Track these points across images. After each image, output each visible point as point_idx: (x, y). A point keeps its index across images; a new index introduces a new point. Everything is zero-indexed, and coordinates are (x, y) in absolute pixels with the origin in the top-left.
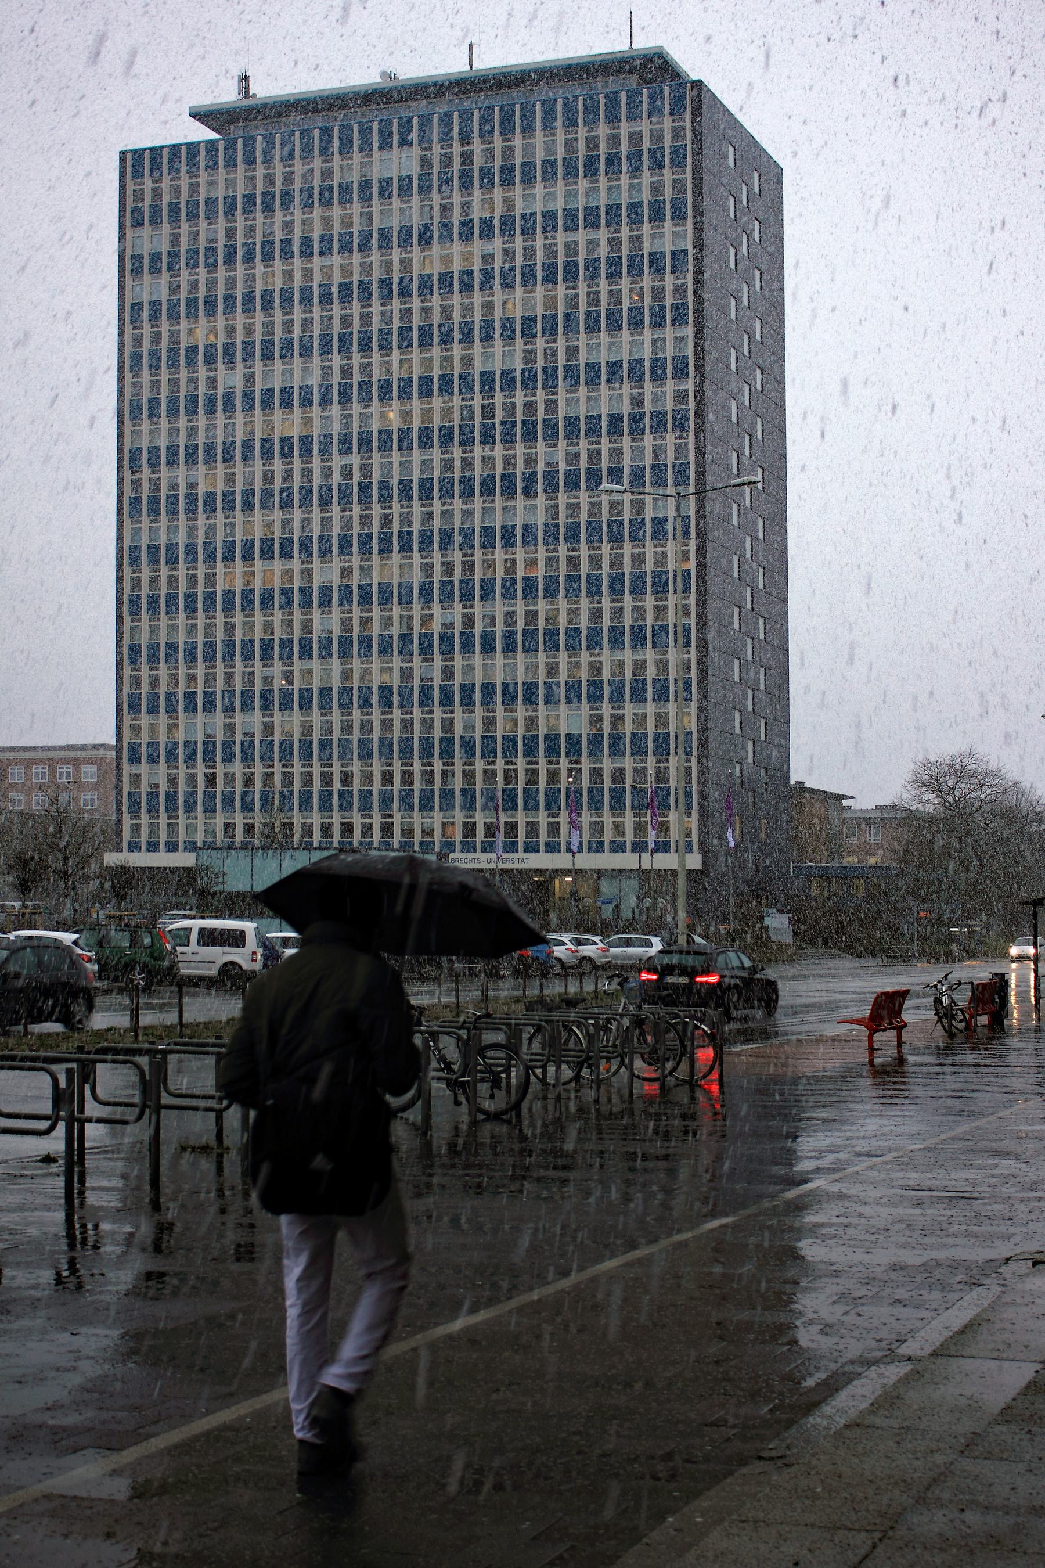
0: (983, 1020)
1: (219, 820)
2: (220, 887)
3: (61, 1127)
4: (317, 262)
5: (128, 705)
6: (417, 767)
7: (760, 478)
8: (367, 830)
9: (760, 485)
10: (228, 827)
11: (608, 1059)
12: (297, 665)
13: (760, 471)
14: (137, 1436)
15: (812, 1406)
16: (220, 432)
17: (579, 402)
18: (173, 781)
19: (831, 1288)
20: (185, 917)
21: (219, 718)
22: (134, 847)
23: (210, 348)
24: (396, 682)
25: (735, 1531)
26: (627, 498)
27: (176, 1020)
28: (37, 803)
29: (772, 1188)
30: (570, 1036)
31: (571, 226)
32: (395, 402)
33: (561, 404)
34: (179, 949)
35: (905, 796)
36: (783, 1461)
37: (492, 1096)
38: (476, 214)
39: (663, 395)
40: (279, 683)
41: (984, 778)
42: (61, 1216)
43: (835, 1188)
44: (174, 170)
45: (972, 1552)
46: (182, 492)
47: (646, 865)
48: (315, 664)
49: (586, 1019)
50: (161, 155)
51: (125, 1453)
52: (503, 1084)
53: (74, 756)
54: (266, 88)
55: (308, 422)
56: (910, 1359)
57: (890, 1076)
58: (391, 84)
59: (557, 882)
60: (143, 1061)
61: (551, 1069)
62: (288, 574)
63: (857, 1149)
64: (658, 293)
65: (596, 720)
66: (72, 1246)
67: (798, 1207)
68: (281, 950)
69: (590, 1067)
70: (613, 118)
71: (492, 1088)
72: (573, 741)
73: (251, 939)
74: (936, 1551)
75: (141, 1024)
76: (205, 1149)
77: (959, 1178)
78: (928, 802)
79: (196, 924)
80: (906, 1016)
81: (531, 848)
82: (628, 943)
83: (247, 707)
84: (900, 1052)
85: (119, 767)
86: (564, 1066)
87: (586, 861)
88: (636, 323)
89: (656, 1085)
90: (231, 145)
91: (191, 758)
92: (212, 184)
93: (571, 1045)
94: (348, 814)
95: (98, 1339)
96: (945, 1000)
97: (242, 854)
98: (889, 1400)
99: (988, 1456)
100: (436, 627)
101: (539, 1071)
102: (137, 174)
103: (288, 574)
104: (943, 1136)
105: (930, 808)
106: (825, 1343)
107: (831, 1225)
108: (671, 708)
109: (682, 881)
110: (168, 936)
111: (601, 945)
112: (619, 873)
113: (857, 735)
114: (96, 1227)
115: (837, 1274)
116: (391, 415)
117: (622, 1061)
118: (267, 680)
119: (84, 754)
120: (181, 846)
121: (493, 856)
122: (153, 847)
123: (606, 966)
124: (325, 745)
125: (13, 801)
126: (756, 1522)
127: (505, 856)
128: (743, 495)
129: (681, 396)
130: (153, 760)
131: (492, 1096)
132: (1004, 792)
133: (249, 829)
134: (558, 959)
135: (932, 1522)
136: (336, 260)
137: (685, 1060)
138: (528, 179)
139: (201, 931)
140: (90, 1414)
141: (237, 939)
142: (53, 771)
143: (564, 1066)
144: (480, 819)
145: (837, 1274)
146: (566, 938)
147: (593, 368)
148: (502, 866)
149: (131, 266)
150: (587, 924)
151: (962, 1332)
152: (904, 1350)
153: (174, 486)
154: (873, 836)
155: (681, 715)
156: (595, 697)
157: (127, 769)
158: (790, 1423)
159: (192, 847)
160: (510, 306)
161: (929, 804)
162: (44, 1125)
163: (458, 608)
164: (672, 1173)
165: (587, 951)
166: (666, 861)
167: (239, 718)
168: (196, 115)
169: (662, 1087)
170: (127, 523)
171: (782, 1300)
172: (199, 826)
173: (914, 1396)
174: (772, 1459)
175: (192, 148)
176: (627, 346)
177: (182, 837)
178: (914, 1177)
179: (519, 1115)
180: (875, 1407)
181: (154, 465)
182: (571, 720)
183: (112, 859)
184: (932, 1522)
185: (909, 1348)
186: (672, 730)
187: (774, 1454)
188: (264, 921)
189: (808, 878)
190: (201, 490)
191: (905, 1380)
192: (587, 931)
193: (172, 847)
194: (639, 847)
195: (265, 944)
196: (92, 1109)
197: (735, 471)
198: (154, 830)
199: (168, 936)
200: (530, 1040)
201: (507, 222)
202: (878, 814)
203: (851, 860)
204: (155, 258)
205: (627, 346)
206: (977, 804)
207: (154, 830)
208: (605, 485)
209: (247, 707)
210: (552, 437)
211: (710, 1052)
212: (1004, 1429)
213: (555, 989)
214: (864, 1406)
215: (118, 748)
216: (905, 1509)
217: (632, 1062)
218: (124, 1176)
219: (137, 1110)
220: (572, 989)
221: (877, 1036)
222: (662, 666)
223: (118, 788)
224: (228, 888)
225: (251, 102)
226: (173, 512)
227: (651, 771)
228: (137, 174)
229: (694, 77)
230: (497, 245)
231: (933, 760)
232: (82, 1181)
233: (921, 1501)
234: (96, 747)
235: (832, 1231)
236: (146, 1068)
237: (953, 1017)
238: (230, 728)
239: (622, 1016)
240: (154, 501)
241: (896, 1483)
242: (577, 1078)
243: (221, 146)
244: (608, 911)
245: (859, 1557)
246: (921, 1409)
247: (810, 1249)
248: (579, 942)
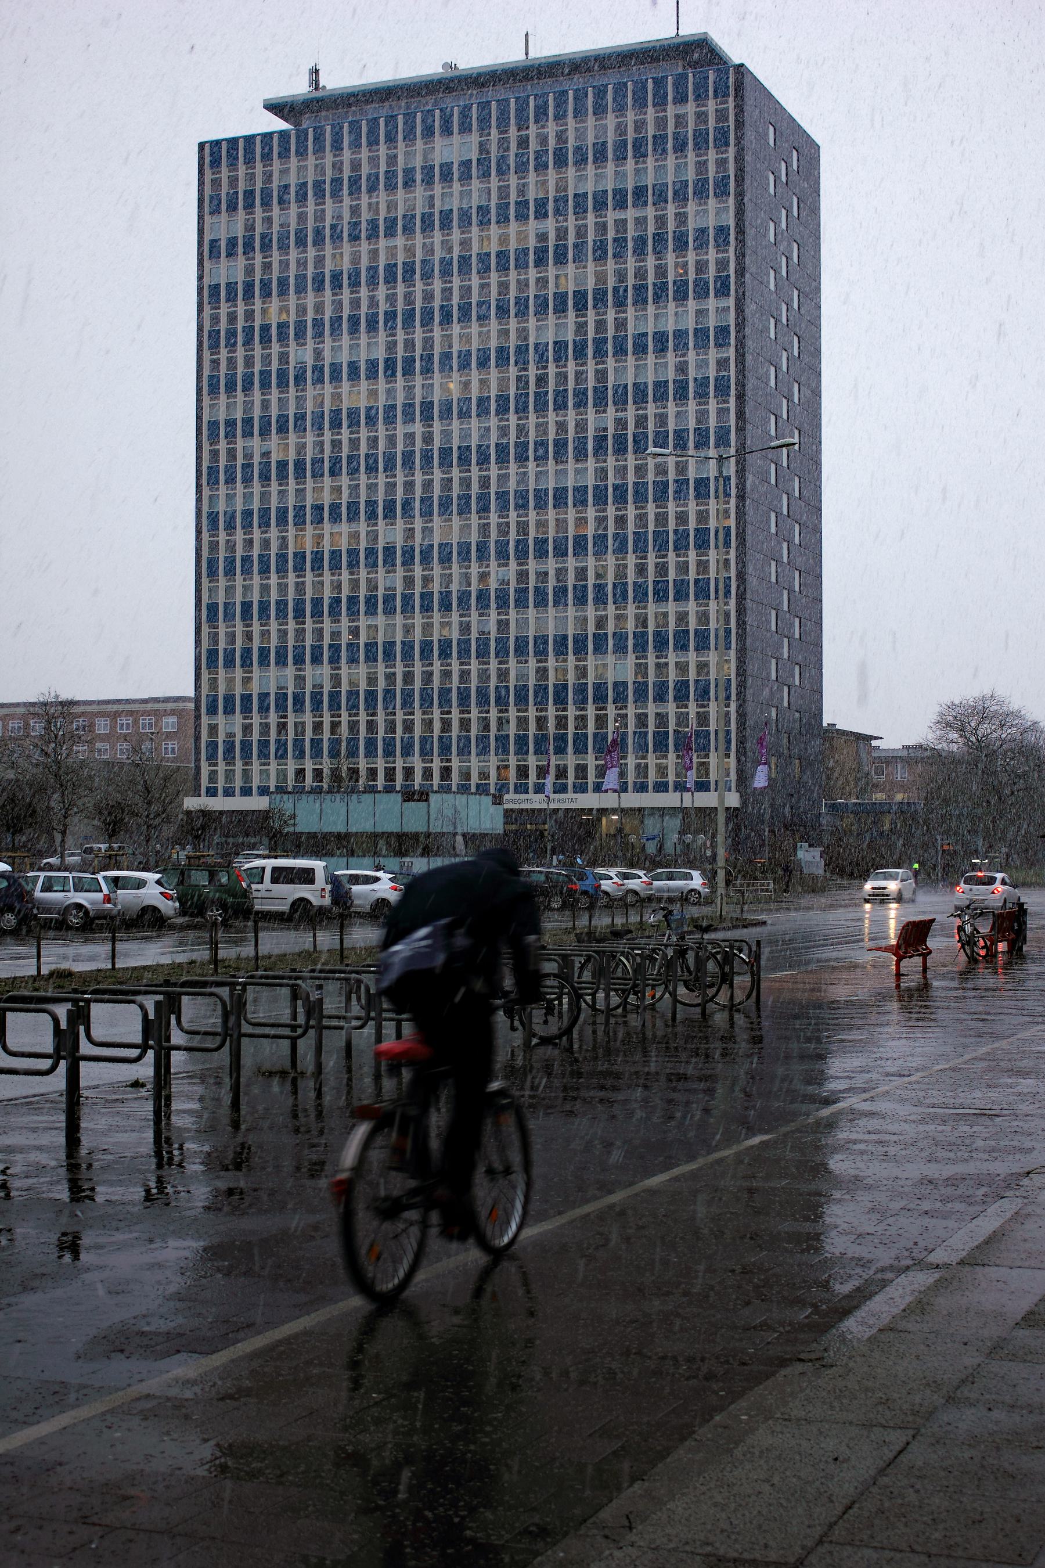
0: (1002, 946)
1: (291, 766)
2: (291, 829)
3: (150, 1053)
4: (383, 243)
5: (207, 660)
7: (796, 440)
8: (428, 774)
9: (796, 447)
10: (300, 773)
11: (654, 987)
12: (363, 622)
13: (796, 433)
14: (226, 1340)
15: (846, 1313)
16: (418, 392)
17: (625, 371)
18: (247, 729)
19: (865, 1198)
20: (258, 856)
21: (290, 671)
22: (212, 792)
23: (282, 326)
24: (455, 636)
25: (778, 1429)
26: (671, 461)
27: (252, 953)
28: (121, 752)
29: (804, 1108)
30: (617, 965)
31: (621, 204)
32: (455, 375)
33: (345, 397)
34: (254, 886)
35: (931, 736)
36: (821, 1363)
37: (546, 1022)
38: (532, 195)
39: (705, 363)
40: (345, 638)
41: (1005, 719)
42: (150, 1135)
43: (866, 1106)
44: (249, 161)
45: (998, 1449)
46: (257, 459)
47: (687, 803)
48: (380, 620)
49: (633, 949)
50: (254, 143)
51: (214, 1357)
52: (556, 1011)
53: (156, 707)
54: (336, 80)
55: (373, 394)
56: (937, 1267)
57: (915, 998)
58: (451, 74)
59: (604, 820)
60: (224, 992)
61: (601, 995)
62: (355, 536)
63: (888, 1069)
64: (701, 267)
65: (641, 669)
66: (160, 1166)
67: (831, 1124)
68: (348, 886)
69: (635, 994)
70: (661, 102)
71: (546, 1015)
72: (620, 687)
73: (320, 876)
74: (965, 1447)
75: (220, 957)
76: (283, 1074)
77: (979, 1097)
78: (952, 741)
79: (270, 863)
80: (932, 943)
81: (581, 788)
82: (670, 877)
83: (317, 660)
84: (925, 978)
85: (198, 717)
86: (612, 993)
87: (632, 800)
88: (681, 296)
89: (698, 1010)
91: (264, 709)
92: (285, 172)
93: (619, 973)
94: (391, 759)
95: (180, 1250)
96: (968, 928)
97: (312, 797)
98: (920, 1306)
99: (1013, 1357)
100: (493, 584)
101: (588, 998)
102: (216, 163)
103: (355, 536)
104: (967, 1057)
105: (954, 747)
106: (855, 1251)
107: (861, 1141)
108: (712, 657)
109: (721, 818)
110: (244, 875)
111: (645, 879)
112: (662, 812)
113: (889, 677)
114: (181, 1148)
115: (869, 1188)
116: (452, 386)
117: (666, 987)
118: (336, 635)
119: (143, 707)
120: (255, 791)
121: (542, 796)
122: (229, 792)
123: (650, 899)
124: (389, 694)
125: (99, 751)
126: (798, 1420)
127: (557, 796)
128: (780, 458)
129: (722, 364)
130: (229, 710)
131: (546, 1022)
132: (1025, 731)
133: (318, 774)
134: (606, 893)
135: (966, 1420)
136: (400, 241)
137: (725, 987)
138: (581, 161)
139: (275, 869)
140: (180, 1320)
141: (306, 876)
142: (136, 723)
143: (612, 993)
144: (532, 761)
145: (869, 1188)
146: (612, 872)
148: (552, 806)
149: (209, 250)
150: (635, 858)
151: (988, 1241)
152: (933, 1258)
153: (248, 456)
154: (900, 774)
155: (722, 662)
156: (641, 647)
157: (205, 720)
158: (825, 1329)
159: (264, 791)
160: (563, 280)
161: (954, 744)
162: (135, 1053)
163: (513, 565)
164: (710, 1092)
165: (632, 884)
166: (706, 800)
167: (309, 669)
169: (703, 1013)
170: (206, 492)
171: (812, 1208)
172: (269, 772)
173: (943, 1302)
174: (811, 1360)
175: (267, 137)
176: (676, 317)
177: (256, 783)
178: (936, 1096)
179: (571, 1041)
180: (907, 1312)
181: (231, 436)
182: (619, 669)
183: (191, 803)
184: (966, 1420)
185: (938, 1256)
186: (712, 678)
187: (813, 1356)
188: (334, 860)
189: (825, 812)
190: (274, 458)
191: (939, 1285)
192: (632, 866)
193: (246, 792)
194: (680, 787)
195: (334, 881)
196: (177, 1038)
197: (773, 433)
198: (229, 775)
199: (244, 875)
200: (582, 968)
201: (561, 201)
202: (905, 753)
203: (879, 797)
204: (232, 242)
205: (676, 317)
206: (998, 743)
207: (229, 775)
208: (651, 449)
209: (317, 660)
210: (600, 401)
211: (748, 978)
212: (1027, 1332)
213: (602, 921)
214: (895, 1311)
215: (197, 700)
216: (936, 1408)
217: (675, 990)
218: (202, 1099)
219: (218, 1039)
220: (619, 921)
221: (904, 963)
222: (704, 618)
223: (197, 738)
224: (298, 829)
226: (247, 480)
227: (692, 716)
228: (216, 163)
229: (737, 61)
230: (550, 225)
231: (957, 702)
232: (168, 1105)
233: (950, 1400)
234: (177, 699)
235: (862, 1147)
236: (227, 999)
237: (975, 944)
238: (300, 680)
239: (666, 946)
240: (230, 470)
241: (928, 1385)
242: (625, 1003)
243: (293, 134)
244: (651, 848)
245: (894, 1453)
246: (950, 1315)
247: (838, 1164)
248: (626, 876)
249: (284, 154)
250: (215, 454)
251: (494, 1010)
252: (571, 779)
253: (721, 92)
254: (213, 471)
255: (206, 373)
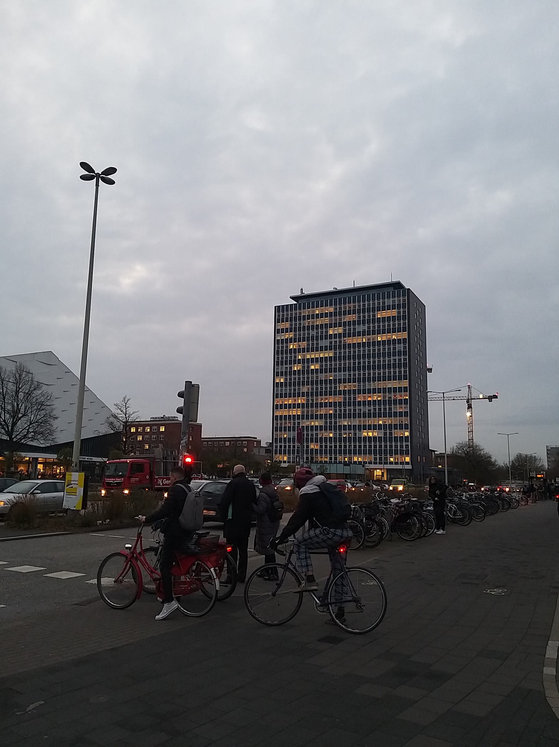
6: (388, 444)
90: (300, 305)
102: (279, 311)
147: (322, 347)
168: (292, 298)
225: (303, 295)
228: (279, 311)
249: (296, 309)
250: (278, 358)
251: (229, 543)
252: (378, 461)
253: (404, 295)
254: (278, 362)
255: (276, 360)
